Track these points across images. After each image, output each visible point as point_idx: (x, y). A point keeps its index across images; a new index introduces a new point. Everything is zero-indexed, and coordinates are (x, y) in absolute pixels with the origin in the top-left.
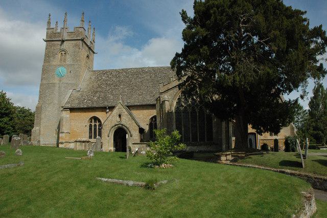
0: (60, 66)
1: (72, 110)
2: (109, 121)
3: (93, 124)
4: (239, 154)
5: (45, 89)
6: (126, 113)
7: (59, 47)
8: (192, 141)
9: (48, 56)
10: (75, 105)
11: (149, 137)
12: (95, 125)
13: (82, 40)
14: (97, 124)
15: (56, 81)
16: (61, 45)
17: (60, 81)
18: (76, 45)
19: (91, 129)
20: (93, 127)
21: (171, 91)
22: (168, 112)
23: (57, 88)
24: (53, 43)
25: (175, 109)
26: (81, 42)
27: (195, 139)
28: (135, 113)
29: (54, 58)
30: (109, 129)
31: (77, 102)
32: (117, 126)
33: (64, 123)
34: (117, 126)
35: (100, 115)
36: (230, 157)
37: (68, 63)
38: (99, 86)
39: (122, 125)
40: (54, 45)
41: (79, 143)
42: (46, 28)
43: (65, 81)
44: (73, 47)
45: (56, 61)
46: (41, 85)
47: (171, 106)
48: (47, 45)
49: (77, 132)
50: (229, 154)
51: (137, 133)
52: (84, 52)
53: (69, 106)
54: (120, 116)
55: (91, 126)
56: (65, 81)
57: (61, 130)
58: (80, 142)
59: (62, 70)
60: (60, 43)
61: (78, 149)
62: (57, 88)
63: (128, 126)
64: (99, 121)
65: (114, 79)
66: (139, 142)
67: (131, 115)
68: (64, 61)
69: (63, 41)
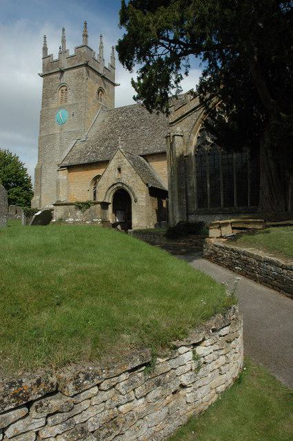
0: (60, 108)
1: (71, 168)
4: (248, 223)
5: (45, 143)
6: (128, 164)
7: (58, 81)
8: (225, 206)
9: (47, 95)
10: (74, 162)
13: (86, 65)
16: (60, 78)
18: (80, 74)
21: (188, 119)
22: (182, 156)
23: (58, 140)
24: (50, 77)
25: (195, 150)
26: (84, 68)
27: (229, 202)
29: (53, 98)
36: (228, 231)
37: (69, 102)
38: (112, 132)
39: (123, 184)
40: (52, 80)
42: (41, 56)
43: (67, 129)
45: (54, 104)
46: (40, 138)
47: (187, 144)
48: (44, 82)
50: (226, 224)
51: (144, 196)
52: (93, 84)
53: (66, 163)
54: (119, 169)
56: (67, 129)
57: (56, 190)
59: (62, 114)
60: (58, 75)
61: (155, 168)
62: (58, 140)
63: (130, 185)
65: (134, 118)
69: (62, 72)
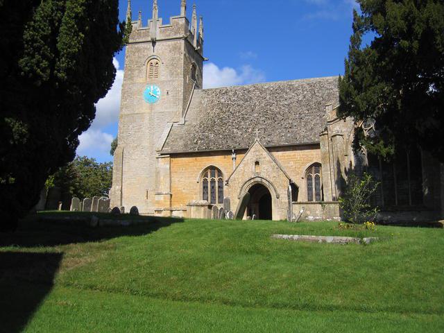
2: (238, 174)
3: (209, 179)
11: (439, 229)
12: (213, 182)
14: (216, 179)
15: (145, 109)
17: (151, 109)
19: (205, 187)
20: (217, 183)
23: (146, 121)
24: (136, 46)
28: (275, 154)
30: (241, 185)
31: (181, 143)
32: (252, 181)
33: (162, 178)
34: (252, 181)
35: (217, 161)
40: (139, 50)
41: (195, 207)
44: (170, 51)
49: (182, 193)
53: (168, 150)
54: (257, 163)
55: (205, 182)
58: (197, 206)
62: (146, 121)
64: (219, 171)
66: (306, 201)
67: (272, 156)
68: (156, 76)
69: (154, 42)
